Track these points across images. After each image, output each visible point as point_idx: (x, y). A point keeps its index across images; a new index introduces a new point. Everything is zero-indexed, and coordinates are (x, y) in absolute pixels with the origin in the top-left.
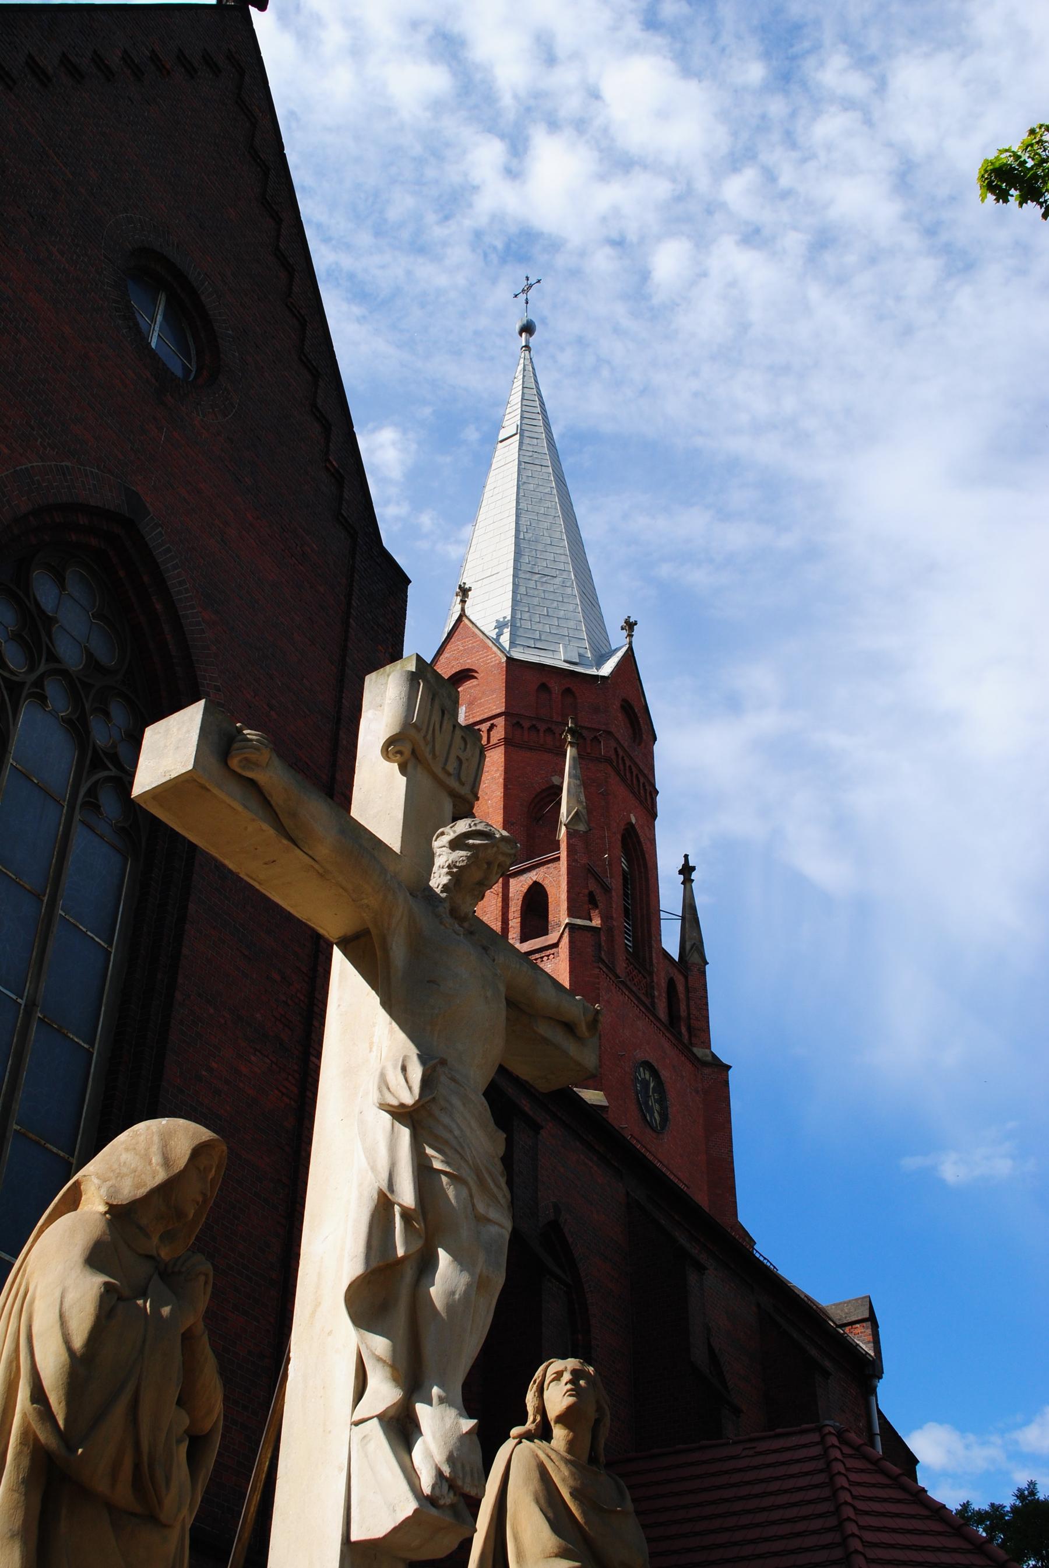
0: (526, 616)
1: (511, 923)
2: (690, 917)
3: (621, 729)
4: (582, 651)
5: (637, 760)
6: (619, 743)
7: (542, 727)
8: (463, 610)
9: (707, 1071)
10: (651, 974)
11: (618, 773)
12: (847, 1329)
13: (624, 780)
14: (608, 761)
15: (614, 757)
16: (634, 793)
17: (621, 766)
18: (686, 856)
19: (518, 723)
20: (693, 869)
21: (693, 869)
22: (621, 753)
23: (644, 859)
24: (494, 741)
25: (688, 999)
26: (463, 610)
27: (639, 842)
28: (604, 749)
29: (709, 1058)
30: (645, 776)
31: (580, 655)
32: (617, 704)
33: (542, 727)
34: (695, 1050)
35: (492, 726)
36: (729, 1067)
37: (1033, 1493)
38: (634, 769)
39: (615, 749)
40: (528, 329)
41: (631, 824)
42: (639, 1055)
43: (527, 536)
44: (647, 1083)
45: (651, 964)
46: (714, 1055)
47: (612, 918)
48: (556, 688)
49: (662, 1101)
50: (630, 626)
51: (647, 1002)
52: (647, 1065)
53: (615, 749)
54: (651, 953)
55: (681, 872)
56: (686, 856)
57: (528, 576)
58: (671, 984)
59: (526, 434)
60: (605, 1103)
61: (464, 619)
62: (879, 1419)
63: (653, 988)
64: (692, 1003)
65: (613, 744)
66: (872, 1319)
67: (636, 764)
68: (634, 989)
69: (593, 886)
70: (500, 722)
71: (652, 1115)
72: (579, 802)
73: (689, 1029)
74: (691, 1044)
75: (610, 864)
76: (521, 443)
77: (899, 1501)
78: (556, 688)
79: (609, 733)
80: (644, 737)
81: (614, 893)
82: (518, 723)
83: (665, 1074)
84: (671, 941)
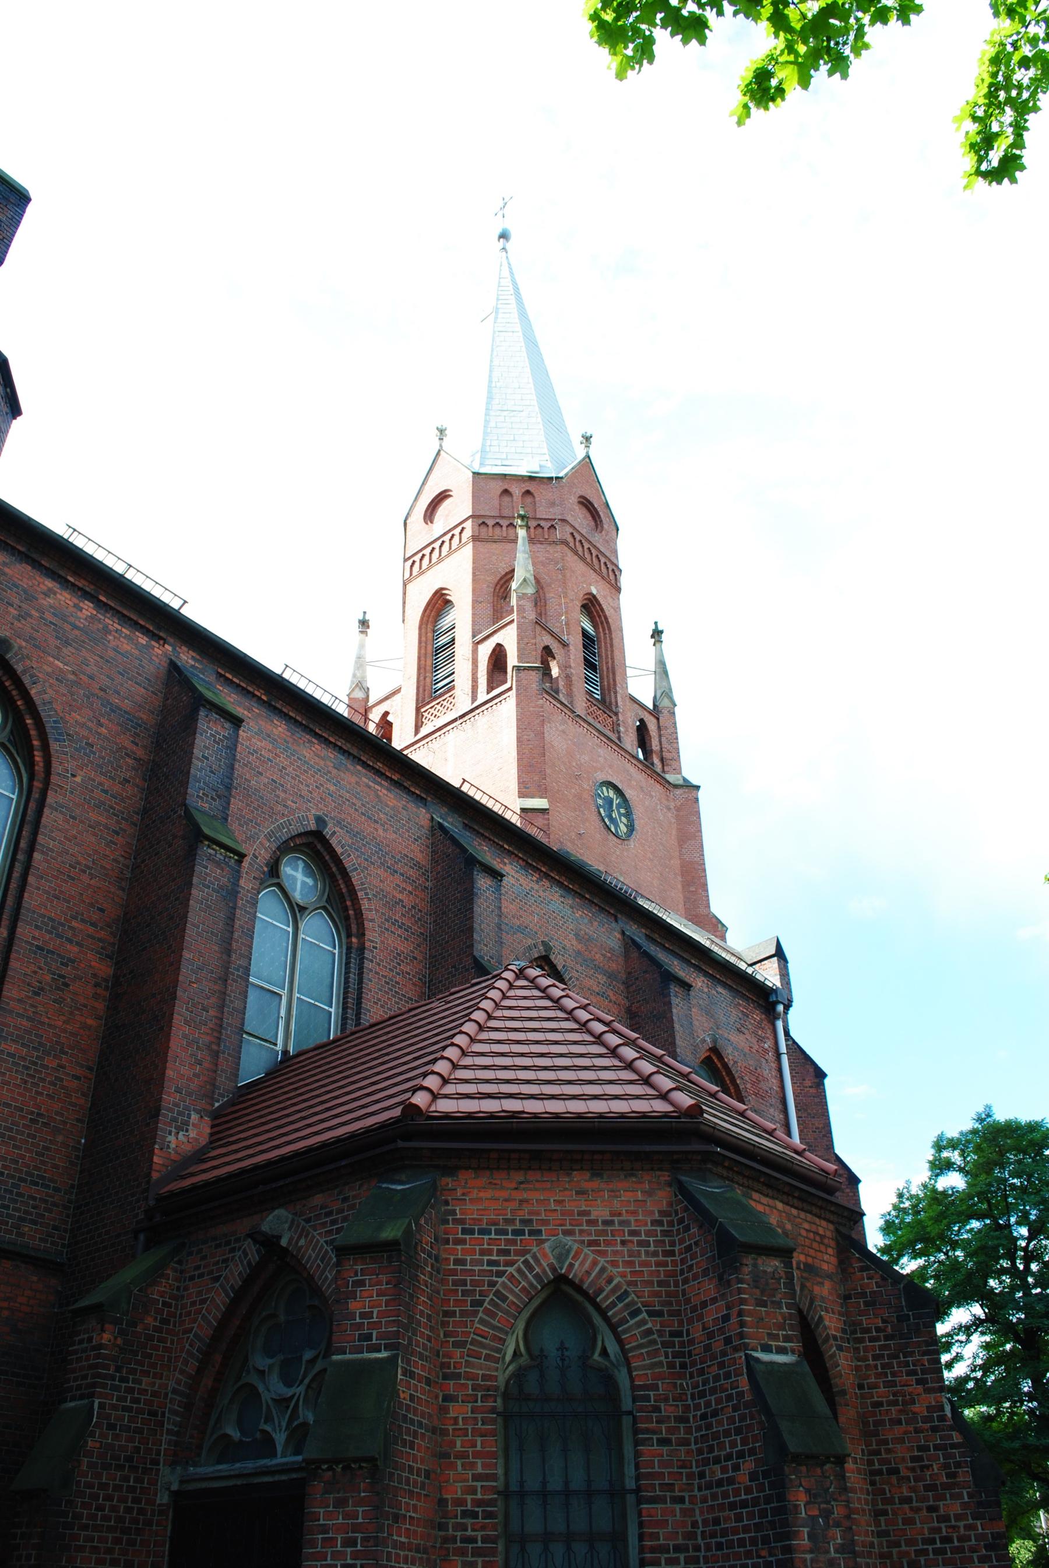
0: (495, 443)
1: (479, 681)
2: (662, 671)
3: (580, 519)
4: (543, 463)
5: (598, 545)
6: (575, 528)
7: (504, 523)
8: (441, 446)
9: (678, 792)
10: (616, 714)
11: (576, 553)
12: (756, 967)
13: (583, 559)
14: (565, 543)
15: (570, 539)
16: (595, 570)
17: (580, 549)
18: (656, 623)
19: (484, 523)
20: (662, 632)
21: (662, 632)
22: (578, 538)
23: (608, 622)
24: (464, 540)
25: (660, 736)
26: (441, 446)
27: (602, 610)
28: (562, 532)
29: (681, 782)
30: (613, 563)
31: (541, 466)
32: (573, 500)
33: (504, 523)
34: (668, 777)
35: (463, 529)
36: (698, 787)
37: (989, 1116)
38: (593, 551)
39: (572, 534)
40: (504, 236)
41: (591, 594)
42: (601, 777)
43: (498, 385)
44: (611, 801)
45: (617, 706)
46: (685, 779)
47: (570, 667)
48: (517, 490)
49: (628, 814)
50: (587, 439)
51: (614, 737)
52: (610, 784)
53: (572, 534)
54: (616, 697)
55: (652, 636)
56: (656, 623)
57: (498, 413)
58: (642, 730)
59: (501, 311)
60: (547, 807)
61: (442, 452)
62: (786, 1040)
63: (619, 725)
64: (663, 739)
65: (569, 530)
66: (779, 953)
67: (595, 547)
68: (598, 726)
69: (547, 640)
70: (468, 525)
71: (617, 826)
72: (528, 571)
73: (662, 760)
74: (664, 771)
75: (567, 624)
76: (496, 318)
77: (546, 1008)
78: (517, 490)
79: (563, 520)
80: (605, 526)
81: (571, 647)
82: (484, 523)
83: (629, 793)
84: (640, 687)
